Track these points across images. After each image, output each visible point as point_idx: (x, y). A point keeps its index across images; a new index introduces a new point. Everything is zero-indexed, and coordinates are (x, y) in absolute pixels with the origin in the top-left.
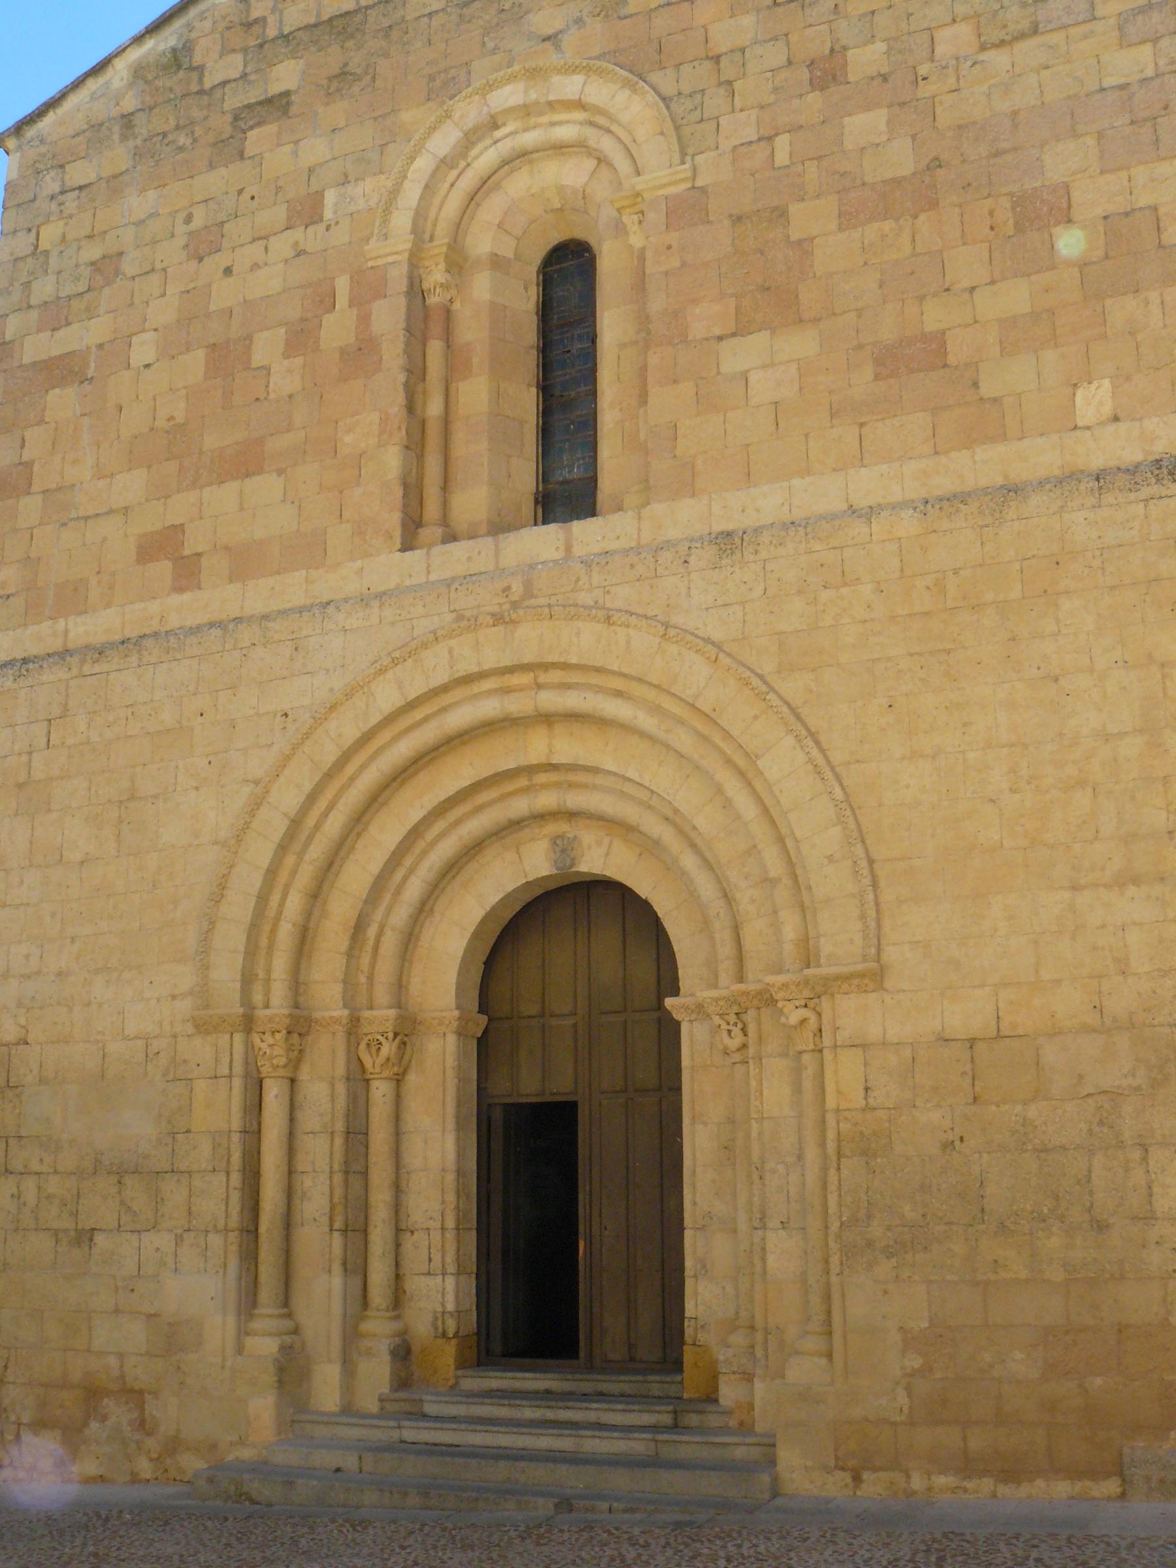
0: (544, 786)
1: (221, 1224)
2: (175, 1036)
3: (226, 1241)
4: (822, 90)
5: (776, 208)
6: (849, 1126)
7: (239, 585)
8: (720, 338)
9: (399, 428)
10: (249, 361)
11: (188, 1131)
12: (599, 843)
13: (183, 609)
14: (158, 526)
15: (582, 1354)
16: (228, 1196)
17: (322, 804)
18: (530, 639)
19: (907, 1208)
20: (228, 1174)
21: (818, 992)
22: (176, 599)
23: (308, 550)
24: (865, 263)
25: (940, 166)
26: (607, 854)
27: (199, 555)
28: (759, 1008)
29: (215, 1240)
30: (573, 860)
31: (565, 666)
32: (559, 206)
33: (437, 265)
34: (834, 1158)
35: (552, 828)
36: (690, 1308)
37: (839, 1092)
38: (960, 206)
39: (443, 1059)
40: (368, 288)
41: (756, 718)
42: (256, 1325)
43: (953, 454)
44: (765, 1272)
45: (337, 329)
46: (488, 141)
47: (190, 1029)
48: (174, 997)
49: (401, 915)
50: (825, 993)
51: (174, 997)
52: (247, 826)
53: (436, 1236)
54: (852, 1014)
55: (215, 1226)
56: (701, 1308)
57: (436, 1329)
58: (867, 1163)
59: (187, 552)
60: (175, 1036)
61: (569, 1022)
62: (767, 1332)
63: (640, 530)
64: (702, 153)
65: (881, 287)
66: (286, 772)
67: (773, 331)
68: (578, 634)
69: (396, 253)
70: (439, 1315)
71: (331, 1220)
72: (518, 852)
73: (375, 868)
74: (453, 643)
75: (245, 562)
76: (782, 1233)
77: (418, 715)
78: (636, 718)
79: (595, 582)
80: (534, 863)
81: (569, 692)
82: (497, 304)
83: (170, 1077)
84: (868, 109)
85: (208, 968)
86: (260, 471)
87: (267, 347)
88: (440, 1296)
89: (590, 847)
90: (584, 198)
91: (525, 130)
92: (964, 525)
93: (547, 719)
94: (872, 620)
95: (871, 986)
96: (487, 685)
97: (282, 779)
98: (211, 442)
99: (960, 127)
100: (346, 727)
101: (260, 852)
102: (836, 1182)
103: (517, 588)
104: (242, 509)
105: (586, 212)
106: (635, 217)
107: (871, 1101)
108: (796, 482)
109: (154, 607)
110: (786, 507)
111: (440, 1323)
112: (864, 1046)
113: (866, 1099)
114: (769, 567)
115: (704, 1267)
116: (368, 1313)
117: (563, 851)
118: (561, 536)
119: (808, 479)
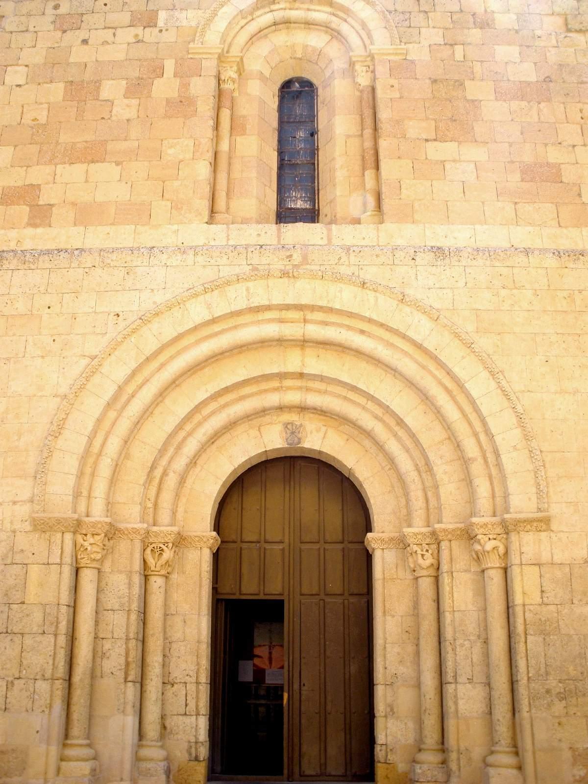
0: (289, 388)
1: (48, 675)
2: (14, 532)
3: (52, 687)
4: (481, 28)
5: (456, 81)
6: (531, 615)
7: (82, 228)
8: (427, 140)
9: (208, 151)
10: (98, 95)
11: (23, 603)
12: (318, 430)
13: (33, 238)
14: (20, 183)
15: (285, 772)
16: (55, 653)
17: (139, 379)
18: (304, 291)
19: (571, 668)
20: (56, 635)
21: (507, 529)
22: (30, 231)
23: (137, 213)
24: (512, 120)
25: (551, 81)
26: (324, 437)
27: (52, 205)
28: (450, 541)
29: (43, 687)
30: (300, 439)
31: (330, 310)
32: (300, 56)
33: (231, 67)
34: (523, 636)
35: (287, 417)
36: (381, 737)
37: (524, 593)
38: (564, 103)
39: (199, 562)
40: (187, 69)
41: (463, 357)
42: (70, 752)
43: (570, 228)
44: (457, 711)
45: (165, 88)
46: (267, 10)
47: (27, 527)
48: (15, 503)
49: (180, 463)
50: (515, 530)
51: (15, 503)
52: (82, 387)
53: (192, 688)
54: (528, 545)
55: (43, 676)
56: (390, 738)
57: (190, 754)
58: (544, 639)
59: (41, 203)
60: (14, 532)
61: (281, 546)
62: (459, 752)
63: (378, 236)
64: (411, 43)
65: (522, 134)
66: (116, 353)
67: (460, 143)
68: (341, 291)
69: (210, 53)
70: (193, 745)
71: (126, 675)
72: (259, 431)
73: (169, 428)
74: (250, 284)
75: (86, 214)
76: (469, 686)
77: (217, 328)
78: (376, 349)
79: (352, 262)
80: (272, 440)
81: (327, 327)
82: (260, 102)
83: (9, 562)
84: (509, 44)
85: (45, 484)
86: (103, 161)
87: (111, 89)
88: (193, 730)
89: (311, 433)
90: (319, 55)
91: (290, 9)
92: (583, 267)
93: (303, 343)
94: (533, 310)
95: (544, 527)
96: (269, 315)
97: (113, 357)
98: (65, 138)
99: (560, 65)
100: (166, 328)
101: (92, 406)
102: (524, 651)
103: (297, 258)
104: (87, 181)
105: (317, 64)
106: (365, 68)
107: (545, 599)
108: (478, 227)
109: (13, 234)
110: (473, 239)
111: (193, 750)
112: (539, 565)
113: (542, 598)
114: (468, 270)
115: (392, 710)
116: (144, 743)
117: (293, 433)
118: (325, 232)
119: (485, 227)
